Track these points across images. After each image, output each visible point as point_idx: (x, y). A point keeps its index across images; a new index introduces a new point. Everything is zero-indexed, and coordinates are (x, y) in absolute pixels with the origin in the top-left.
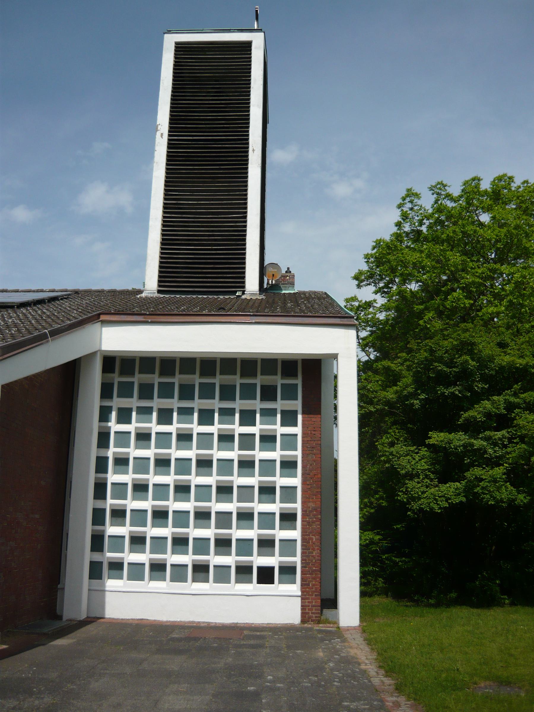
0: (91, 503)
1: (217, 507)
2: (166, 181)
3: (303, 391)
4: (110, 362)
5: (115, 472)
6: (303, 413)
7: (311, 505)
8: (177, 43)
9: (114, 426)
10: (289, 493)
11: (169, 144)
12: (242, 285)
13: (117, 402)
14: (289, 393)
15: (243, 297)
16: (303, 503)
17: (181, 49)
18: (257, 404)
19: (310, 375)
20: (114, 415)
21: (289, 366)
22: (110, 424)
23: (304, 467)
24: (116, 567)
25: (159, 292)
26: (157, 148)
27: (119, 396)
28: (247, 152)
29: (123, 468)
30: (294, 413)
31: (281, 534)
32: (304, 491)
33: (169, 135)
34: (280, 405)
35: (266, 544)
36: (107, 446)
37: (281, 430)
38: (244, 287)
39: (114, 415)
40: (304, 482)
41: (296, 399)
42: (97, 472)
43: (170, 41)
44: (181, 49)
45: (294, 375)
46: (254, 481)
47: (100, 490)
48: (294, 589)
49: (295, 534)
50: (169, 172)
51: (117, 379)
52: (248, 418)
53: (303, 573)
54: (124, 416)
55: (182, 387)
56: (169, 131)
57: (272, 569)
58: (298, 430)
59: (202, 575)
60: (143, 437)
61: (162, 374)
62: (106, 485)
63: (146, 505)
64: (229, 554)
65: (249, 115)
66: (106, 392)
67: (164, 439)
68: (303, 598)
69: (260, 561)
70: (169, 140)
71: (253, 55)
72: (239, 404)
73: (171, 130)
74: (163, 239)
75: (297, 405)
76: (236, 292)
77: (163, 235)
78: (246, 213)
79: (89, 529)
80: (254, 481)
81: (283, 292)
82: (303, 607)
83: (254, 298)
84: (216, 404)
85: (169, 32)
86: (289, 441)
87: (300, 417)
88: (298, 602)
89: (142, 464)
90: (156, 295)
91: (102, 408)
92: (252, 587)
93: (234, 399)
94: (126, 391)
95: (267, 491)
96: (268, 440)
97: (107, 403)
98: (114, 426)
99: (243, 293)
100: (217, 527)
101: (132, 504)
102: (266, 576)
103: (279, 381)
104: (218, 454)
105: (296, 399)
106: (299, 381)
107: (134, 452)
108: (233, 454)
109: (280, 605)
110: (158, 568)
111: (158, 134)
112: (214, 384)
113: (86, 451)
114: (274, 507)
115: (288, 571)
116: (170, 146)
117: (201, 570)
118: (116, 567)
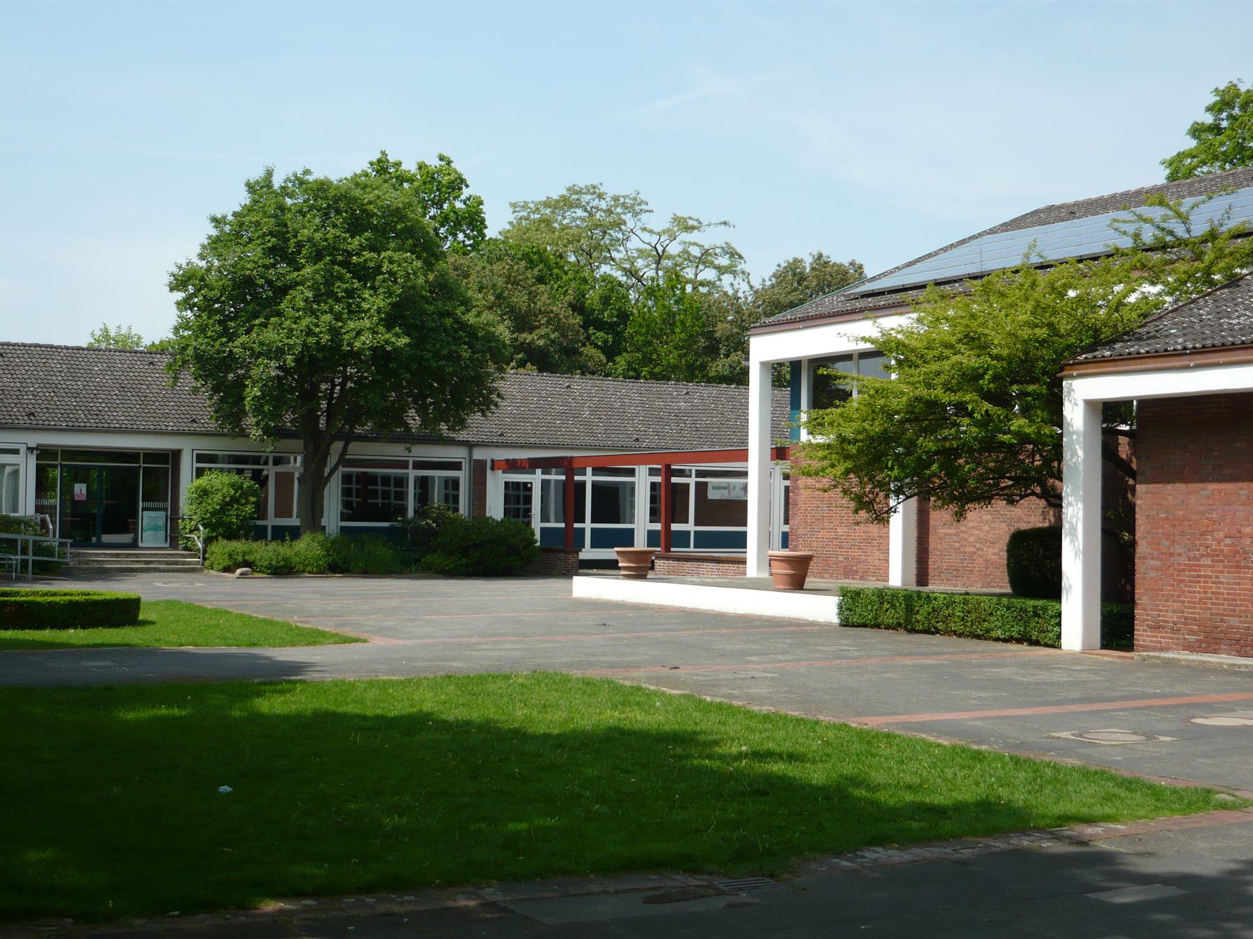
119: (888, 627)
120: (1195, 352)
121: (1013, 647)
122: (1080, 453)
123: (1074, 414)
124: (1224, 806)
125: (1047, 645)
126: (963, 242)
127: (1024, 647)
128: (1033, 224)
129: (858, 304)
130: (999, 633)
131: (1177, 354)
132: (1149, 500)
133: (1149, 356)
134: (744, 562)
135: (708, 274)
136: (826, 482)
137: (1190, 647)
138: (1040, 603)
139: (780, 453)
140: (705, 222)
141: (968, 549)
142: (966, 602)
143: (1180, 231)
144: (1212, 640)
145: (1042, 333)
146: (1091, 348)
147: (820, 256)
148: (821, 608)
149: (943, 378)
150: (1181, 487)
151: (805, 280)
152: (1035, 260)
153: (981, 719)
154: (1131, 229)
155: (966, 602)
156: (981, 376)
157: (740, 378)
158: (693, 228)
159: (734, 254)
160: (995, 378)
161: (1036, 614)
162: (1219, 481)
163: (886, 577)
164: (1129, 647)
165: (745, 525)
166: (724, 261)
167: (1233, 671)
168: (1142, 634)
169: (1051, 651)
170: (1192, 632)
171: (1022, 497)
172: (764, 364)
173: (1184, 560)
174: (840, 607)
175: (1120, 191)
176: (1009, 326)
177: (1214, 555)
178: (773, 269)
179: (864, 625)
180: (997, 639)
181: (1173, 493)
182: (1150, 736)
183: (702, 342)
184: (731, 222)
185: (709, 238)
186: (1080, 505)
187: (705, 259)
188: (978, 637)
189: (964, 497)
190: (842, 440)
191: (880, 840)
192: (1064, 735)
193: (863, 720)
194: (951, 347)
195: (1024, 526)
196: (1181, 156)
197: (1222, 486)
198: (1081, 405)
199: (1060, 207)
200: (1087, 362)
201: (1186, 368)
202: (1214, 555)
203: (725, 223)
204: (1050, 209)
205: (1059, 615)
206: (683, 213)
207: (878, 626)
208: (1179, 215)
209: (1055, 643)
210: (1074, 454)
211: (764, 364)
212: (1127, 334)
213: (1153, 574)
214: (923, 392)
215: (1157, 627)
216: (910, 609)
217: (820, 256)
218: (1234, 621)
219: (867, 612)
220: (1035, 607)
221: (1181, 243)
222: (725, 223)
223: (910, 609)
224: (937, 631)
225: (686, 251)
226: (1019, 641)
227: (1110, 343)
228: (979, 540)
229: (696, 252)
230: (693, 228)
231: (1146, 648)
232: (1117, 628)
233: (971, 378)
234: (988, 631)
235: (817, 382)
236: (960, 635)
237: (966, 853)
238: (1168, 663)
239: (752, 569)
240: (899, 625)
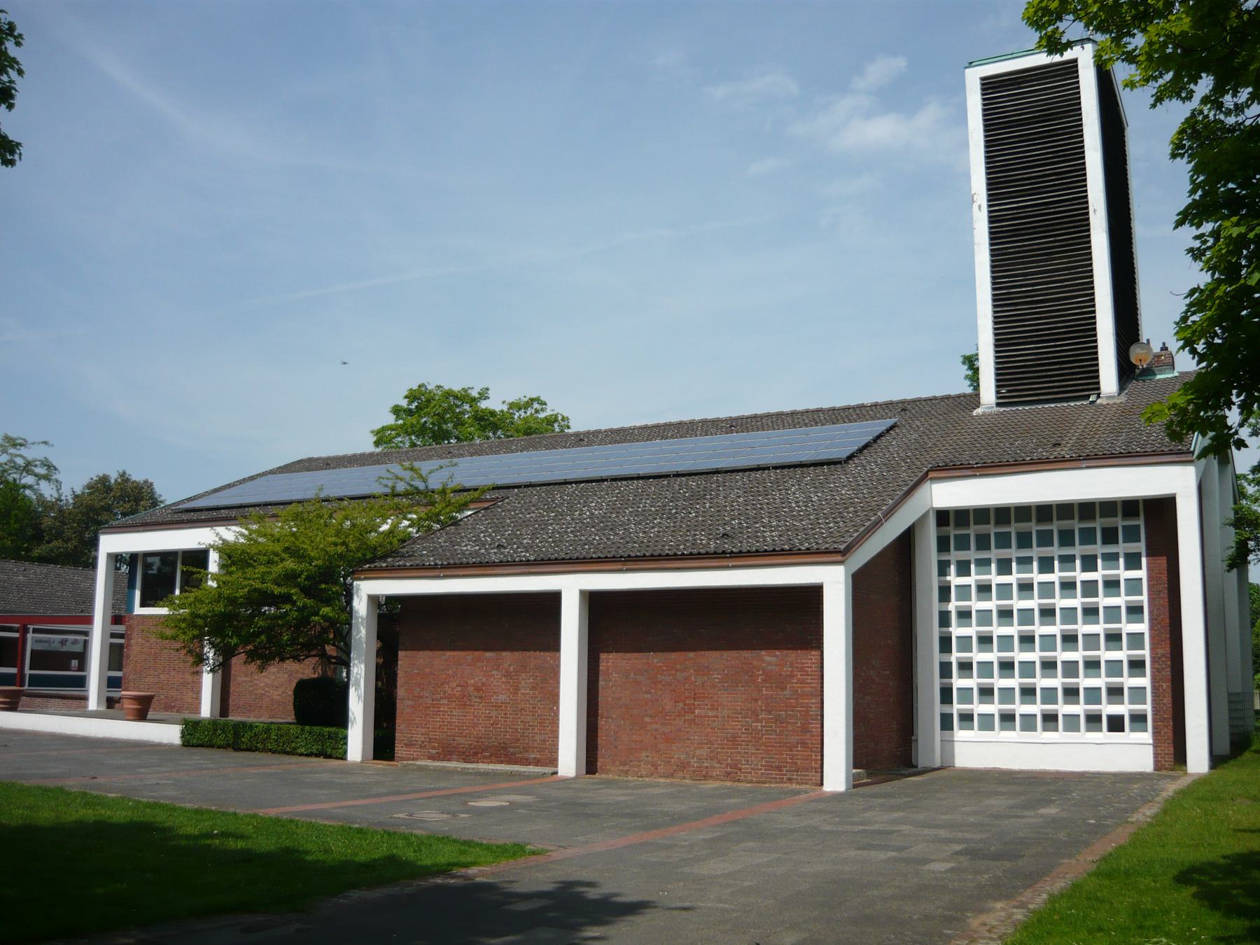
0: (937, 657)
1: (1062, 656)
2: (992, 267)
3: (1146, 533)
4: (943, 516)
5: (959, 625)
6: (1148, 555)
7: (1160, 651)
8: (983, 79)
9: (954, 580)
10: (1136, 640)
11: (990, 217)
12: (1096, 387)
13: (954, 555)
14: (1132, 535)
15: (1099, 401)
16: (1152, 649)
17: (989, 85)
18: (1098, 549)
19: (1160, 512)
20: (953, 568)
21: (1130, 507)
22: (948, 578)
23: (1151, 613)
24: (967, 718)
25: (998, 405)
26: (976, 225)
27: (956, 549)
28: (1087, 213)
29: (966, 620)
30: (1139, 555)
31: (1129, 682)
32: (1152, 638)
33: (989, 206)
34: (1122, 548)
35: (1115, 693)
36: (949, 600)
37: (1124, 574)
38: (1099, 389)
39: (953, 568)
40: (1152, 628)
41: (1139, 541)
42: (941, 626)
43: (973, 78)
44: (989, 85)
45: (1136, 515)
46: (1099, 628)
47: (946, 644)
48: (1147, 737)
49: (1145, 682)
50: (994, 254)
51: (952, 532)
52: (1089, 564)
53: (1154, 720)
54: (964, 569)
55: (1019, 535)
56: (989, 201)
57: (1122, 717)
58: (1142, 574)
59: (1052, 724)
60: (984, 589)
61: (998, 523)
62: (950, 638)
63: (993, 656)
64: (1035, 703)
65: (1084, 163)
66: (943, 545)
67: (1005, 590)
68: (1155, 746)
69: (1108, 709)
70: (990, 212)
71: (1081, 79)
72: (1078, 550)
73: (991, 198)
74: (996, 340)
75: (1141, 547)
76: (1089, 396)
77: (996, 335)
78: (1093, 294)
79: (937, 682)
80: (1099, 628)
81: (1158, 377)
82: (1156, 755)
83: (1111, 402)
84: (1055, 551)
85: (971, 64)
86: (1134, 586)
87: (1144, 560)
88: (1150, 749)
89: (985, 617)
90: (996, 409)
91: (939, 562)
92: (1104, 735)
93: (1073, 545)
94: (963, 544)
95: (1114, 638)
96: (1112, 585)
97: (945, 557)
98: (954, 580)
99: (1099, 396)
100: (1107, 676)
101: (978, 656)
102: (1116, 724)
103: (1120, 523)
104: (1060, 602)
105: (1139, 541)
106: (1141, 522)
107: (976, 605)
108: (1077, 602)
109: (1133, 752)
110: (1007, 718)
111: (975, 206)
112: (1052, 531)
113: (927, 605)
114: (1122, 655)
115: (1138, 719)
116: (992, 220)
117: (1050, 720)
118: (967, 718)
119: (219, 747)
120: (443, 567)
121: (314, 759)
122: (363, 631)
123: (360, 606)
124: (533, 853)
125: (337, 758)
126: (252, 478)
127: (321, 759)
128: (301, 470)
129: (185, 517)
130: (303, 750)
131: (430, 568)
132: (406, 661)
133: (412, 568)
134: (85, 698)
135: (29, 480)
136: (178, 645)
137: (432, 758)
138: (333, 729)
139: (117, 620)
140: (30, 441)
141: (260, 691)
142: (279, 729)
143: (421, 486)
144: (447, 753)
145: (340, 549)
146: (372, 561)
147: (124, 473)
148: (170, 734)
149: (274, 576)
150: (428, 653)
151: (111, 490)
152: (323, 495)
153: (343, 807)
154: (390, 484)
155: (279, 729)
156: (299, 576)
157: (93, 565)
158: (21, 445)
159: (49, 466)
160: (308, 578)
161: (330, 737)
162: (454, 650)
163: (197, 709)
164: (390, 757)
165: (980, 729)
166: (41, 471)
167: (463, 772)
168: (400, 750)
169: (341, 762)
170: (433, 748)
171: (307, 657)
172: (110, 555)
173: (429, 701)
174: (183, 732)
175: (359, 452)
176: (321, 544)
177: (449, 698)
178: (86, 481)
179: (202, 746)
180: (301, 755)
181: (423, 657)
182: (454, 815)
183: (30, 532)
184: (51, 442)
185: (30, 453)
186: (363, 666)
187: (28, 468)
188: (288, 753)
189: (263, 656)
190: (195, 616)
191: (354, 886)
192: (401, 816)
193: (267, 810)
194: (277, 555)
195: (305, 677)
196: (384, 429)
197: (456, 653)
198: (365, 599)
199: (317, 459)
200: (370, 570)
201: (438, 577)
202: (449, 698)
203: (46, 443)
204: (310, 460)
205: (346, 738)
206: (12, 435)
207: (212, 746)
208: (421, 476)
209: (343, 756)
210: (359, 632)
211: (110, 555)
212: (393, 553)
213: (408, 710)
214: (258, 585)
215: (410, 745)
216: (237, 735)
217: (124, 473)
218: (461, 740)
219: (196, 736)
220: (329, 733)
221: (419, 492)
222: (46, 443)
223: (237, 735)
224: (257, 749)
225: (11, 461)
226: (317, 755)
227: (384, 557)
228: (267, 685)
229: (20, 461)
230: (21, 445)
231: (403, 759)
232: (383, 746)
233: (291, 577)
234: (295, 749)
235: (157, 575)
236: (274, 752)
237: (408, 890)
238: (421, 768)
239: (93, 704)
240: (228, 745)
